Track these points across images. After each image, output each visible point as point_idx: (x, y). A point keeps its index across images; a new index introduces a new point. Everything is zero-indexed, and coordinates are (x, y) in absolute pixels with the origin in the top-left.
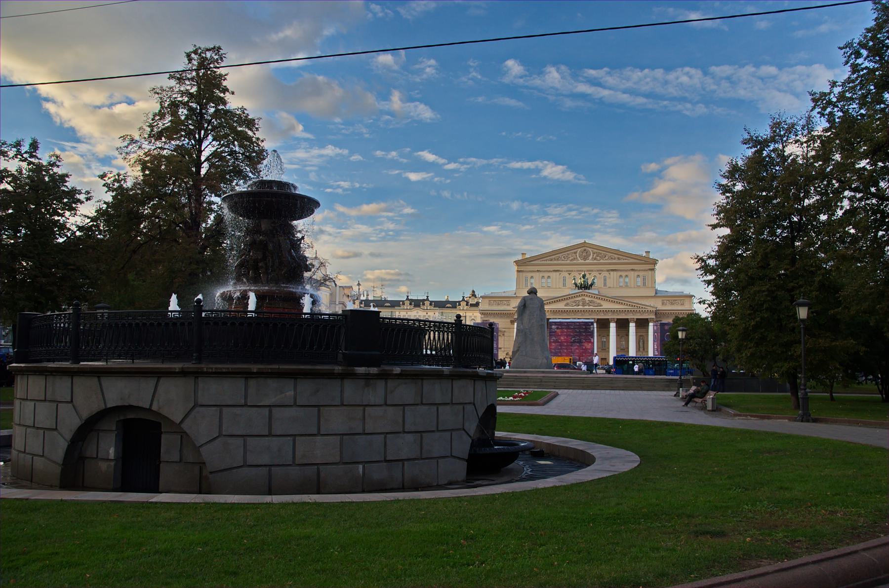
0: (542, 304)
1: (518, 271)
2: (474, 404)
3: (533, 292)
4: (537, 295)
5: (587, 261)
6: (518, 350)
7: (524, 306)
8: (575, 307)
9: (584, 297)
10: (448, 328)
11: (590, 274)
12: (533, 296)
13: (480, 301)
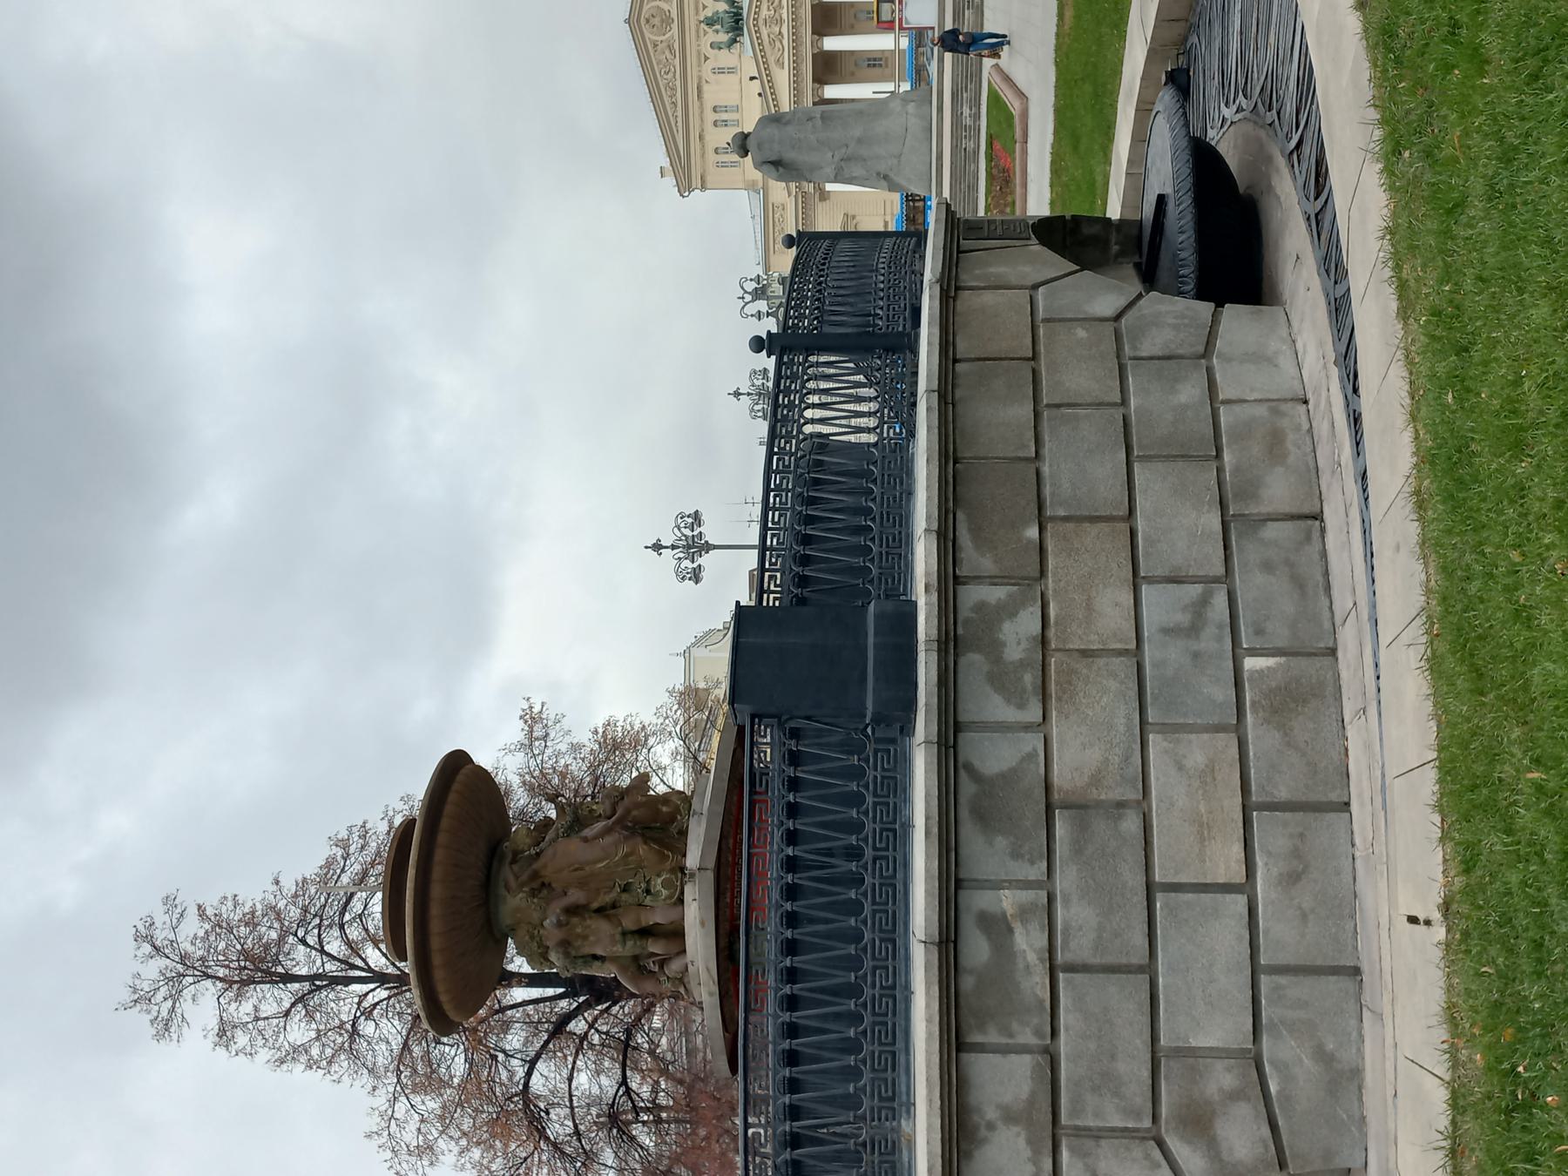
0: (774, 119)
1: (703, 187)
2: (1035, 287)
3: (742, 144)
4: (749, 134)
5: (674, 14)
6: (886, 177)
7: (779, 166)
8: (785, 42)
9: (761, 22)
10: (794, 377)
11: (705, 7)
12: (751, 143)
13: (776, 275)
